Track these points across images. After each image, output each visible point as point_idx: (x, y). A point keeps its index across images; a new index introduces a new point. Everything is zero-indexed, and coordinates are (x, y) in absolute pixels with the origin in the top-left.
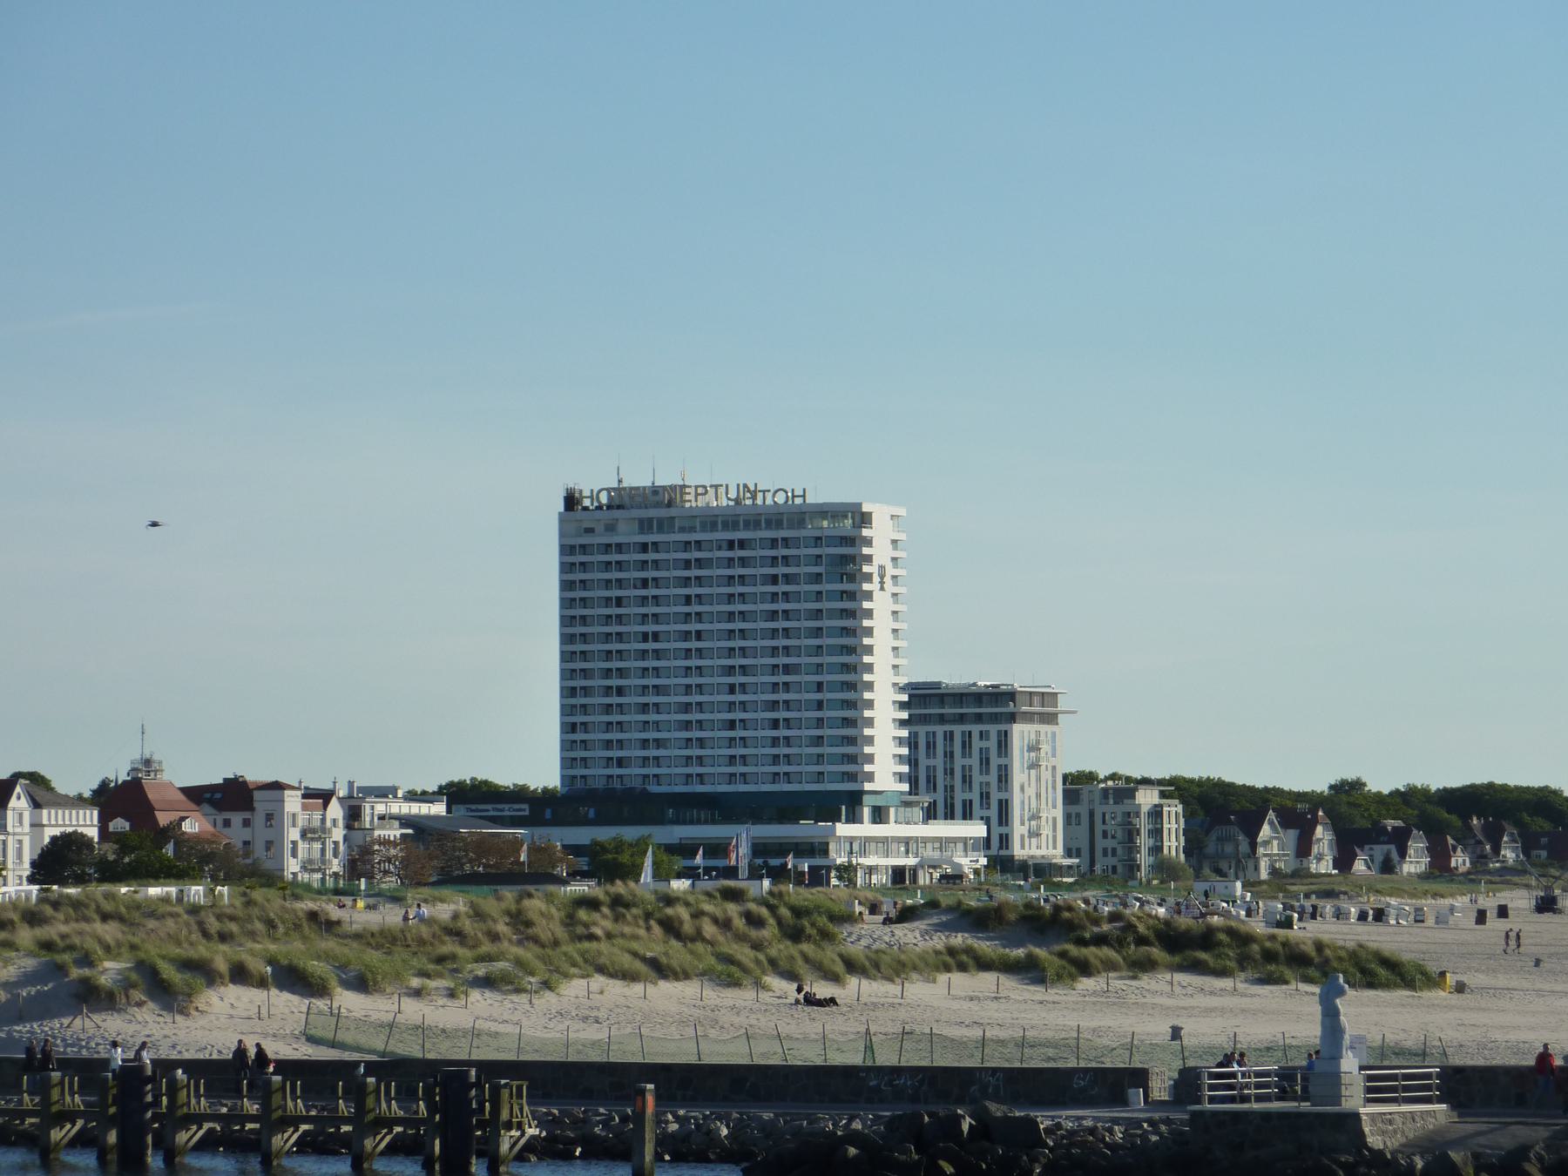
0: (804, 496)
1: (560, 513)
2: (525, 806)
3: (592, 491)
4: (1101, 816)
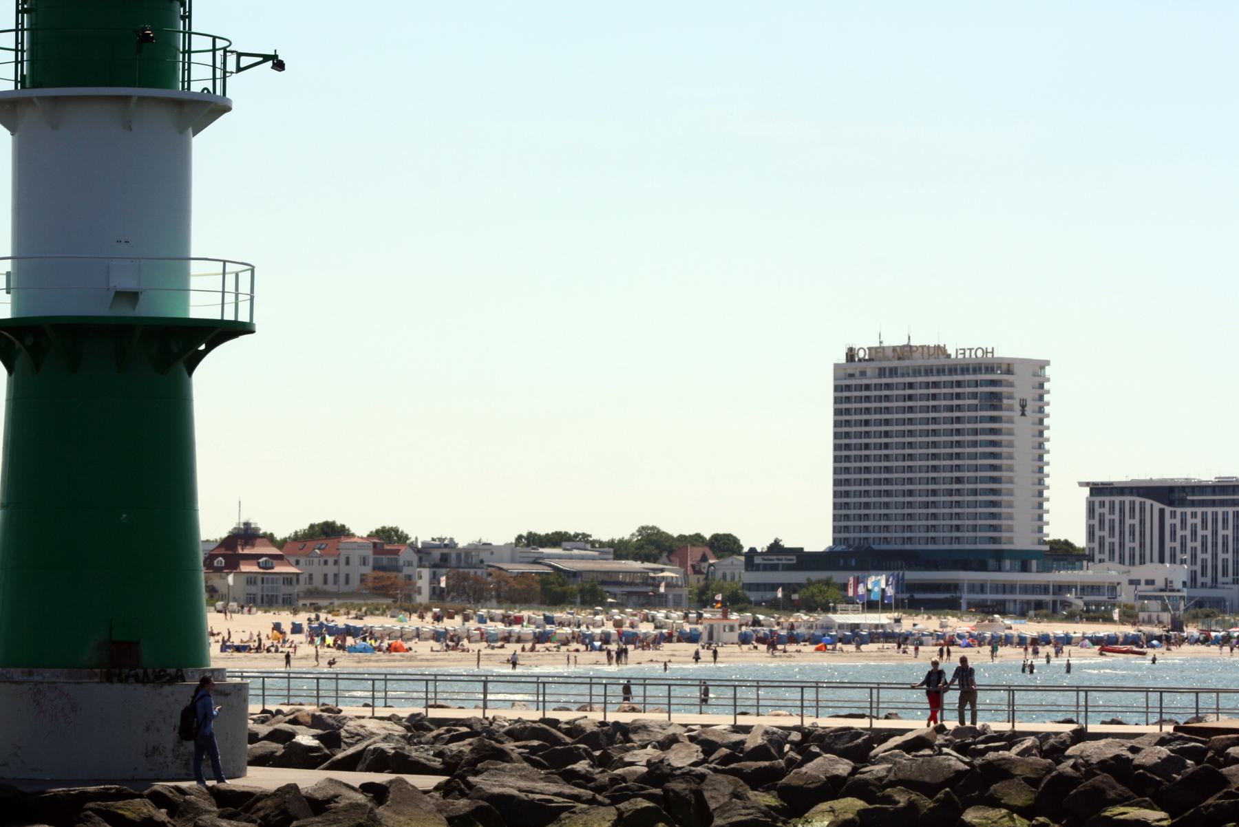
0: (992, 352)
1: (837, 366)
2: (794, 557)
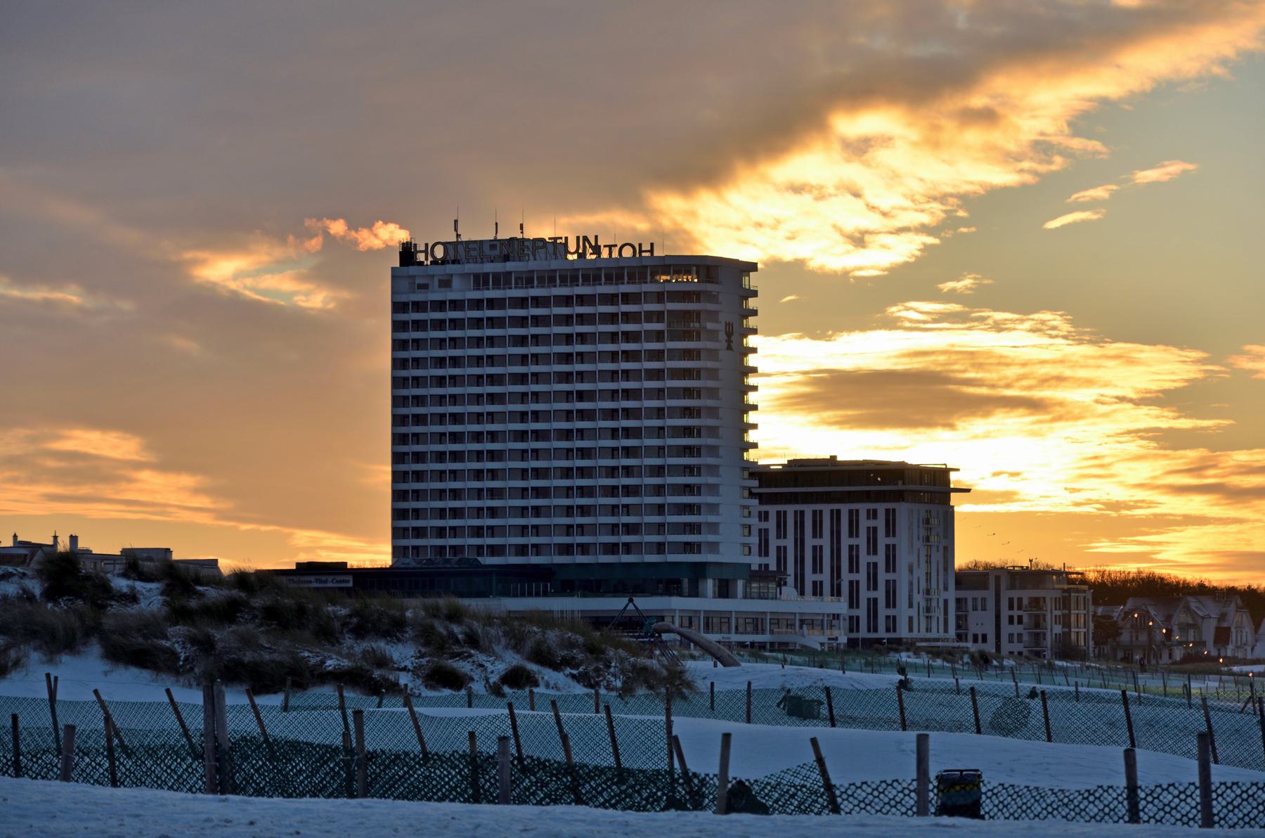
0: (651, 251)
3: (427, 245)
4: (921, 566)
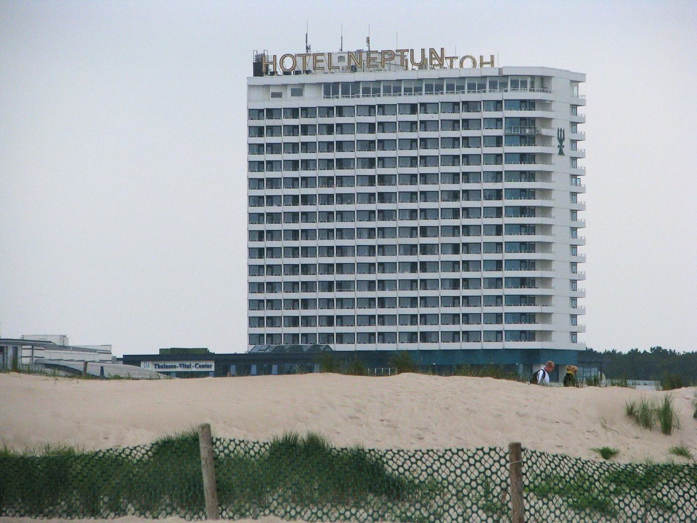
0: (492, 63)
3: (275, 57)
